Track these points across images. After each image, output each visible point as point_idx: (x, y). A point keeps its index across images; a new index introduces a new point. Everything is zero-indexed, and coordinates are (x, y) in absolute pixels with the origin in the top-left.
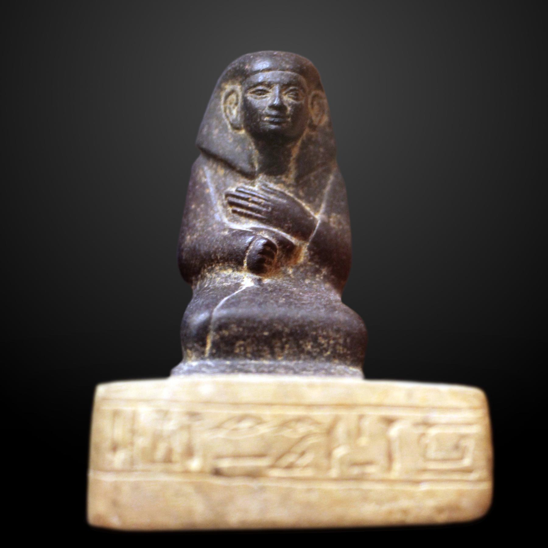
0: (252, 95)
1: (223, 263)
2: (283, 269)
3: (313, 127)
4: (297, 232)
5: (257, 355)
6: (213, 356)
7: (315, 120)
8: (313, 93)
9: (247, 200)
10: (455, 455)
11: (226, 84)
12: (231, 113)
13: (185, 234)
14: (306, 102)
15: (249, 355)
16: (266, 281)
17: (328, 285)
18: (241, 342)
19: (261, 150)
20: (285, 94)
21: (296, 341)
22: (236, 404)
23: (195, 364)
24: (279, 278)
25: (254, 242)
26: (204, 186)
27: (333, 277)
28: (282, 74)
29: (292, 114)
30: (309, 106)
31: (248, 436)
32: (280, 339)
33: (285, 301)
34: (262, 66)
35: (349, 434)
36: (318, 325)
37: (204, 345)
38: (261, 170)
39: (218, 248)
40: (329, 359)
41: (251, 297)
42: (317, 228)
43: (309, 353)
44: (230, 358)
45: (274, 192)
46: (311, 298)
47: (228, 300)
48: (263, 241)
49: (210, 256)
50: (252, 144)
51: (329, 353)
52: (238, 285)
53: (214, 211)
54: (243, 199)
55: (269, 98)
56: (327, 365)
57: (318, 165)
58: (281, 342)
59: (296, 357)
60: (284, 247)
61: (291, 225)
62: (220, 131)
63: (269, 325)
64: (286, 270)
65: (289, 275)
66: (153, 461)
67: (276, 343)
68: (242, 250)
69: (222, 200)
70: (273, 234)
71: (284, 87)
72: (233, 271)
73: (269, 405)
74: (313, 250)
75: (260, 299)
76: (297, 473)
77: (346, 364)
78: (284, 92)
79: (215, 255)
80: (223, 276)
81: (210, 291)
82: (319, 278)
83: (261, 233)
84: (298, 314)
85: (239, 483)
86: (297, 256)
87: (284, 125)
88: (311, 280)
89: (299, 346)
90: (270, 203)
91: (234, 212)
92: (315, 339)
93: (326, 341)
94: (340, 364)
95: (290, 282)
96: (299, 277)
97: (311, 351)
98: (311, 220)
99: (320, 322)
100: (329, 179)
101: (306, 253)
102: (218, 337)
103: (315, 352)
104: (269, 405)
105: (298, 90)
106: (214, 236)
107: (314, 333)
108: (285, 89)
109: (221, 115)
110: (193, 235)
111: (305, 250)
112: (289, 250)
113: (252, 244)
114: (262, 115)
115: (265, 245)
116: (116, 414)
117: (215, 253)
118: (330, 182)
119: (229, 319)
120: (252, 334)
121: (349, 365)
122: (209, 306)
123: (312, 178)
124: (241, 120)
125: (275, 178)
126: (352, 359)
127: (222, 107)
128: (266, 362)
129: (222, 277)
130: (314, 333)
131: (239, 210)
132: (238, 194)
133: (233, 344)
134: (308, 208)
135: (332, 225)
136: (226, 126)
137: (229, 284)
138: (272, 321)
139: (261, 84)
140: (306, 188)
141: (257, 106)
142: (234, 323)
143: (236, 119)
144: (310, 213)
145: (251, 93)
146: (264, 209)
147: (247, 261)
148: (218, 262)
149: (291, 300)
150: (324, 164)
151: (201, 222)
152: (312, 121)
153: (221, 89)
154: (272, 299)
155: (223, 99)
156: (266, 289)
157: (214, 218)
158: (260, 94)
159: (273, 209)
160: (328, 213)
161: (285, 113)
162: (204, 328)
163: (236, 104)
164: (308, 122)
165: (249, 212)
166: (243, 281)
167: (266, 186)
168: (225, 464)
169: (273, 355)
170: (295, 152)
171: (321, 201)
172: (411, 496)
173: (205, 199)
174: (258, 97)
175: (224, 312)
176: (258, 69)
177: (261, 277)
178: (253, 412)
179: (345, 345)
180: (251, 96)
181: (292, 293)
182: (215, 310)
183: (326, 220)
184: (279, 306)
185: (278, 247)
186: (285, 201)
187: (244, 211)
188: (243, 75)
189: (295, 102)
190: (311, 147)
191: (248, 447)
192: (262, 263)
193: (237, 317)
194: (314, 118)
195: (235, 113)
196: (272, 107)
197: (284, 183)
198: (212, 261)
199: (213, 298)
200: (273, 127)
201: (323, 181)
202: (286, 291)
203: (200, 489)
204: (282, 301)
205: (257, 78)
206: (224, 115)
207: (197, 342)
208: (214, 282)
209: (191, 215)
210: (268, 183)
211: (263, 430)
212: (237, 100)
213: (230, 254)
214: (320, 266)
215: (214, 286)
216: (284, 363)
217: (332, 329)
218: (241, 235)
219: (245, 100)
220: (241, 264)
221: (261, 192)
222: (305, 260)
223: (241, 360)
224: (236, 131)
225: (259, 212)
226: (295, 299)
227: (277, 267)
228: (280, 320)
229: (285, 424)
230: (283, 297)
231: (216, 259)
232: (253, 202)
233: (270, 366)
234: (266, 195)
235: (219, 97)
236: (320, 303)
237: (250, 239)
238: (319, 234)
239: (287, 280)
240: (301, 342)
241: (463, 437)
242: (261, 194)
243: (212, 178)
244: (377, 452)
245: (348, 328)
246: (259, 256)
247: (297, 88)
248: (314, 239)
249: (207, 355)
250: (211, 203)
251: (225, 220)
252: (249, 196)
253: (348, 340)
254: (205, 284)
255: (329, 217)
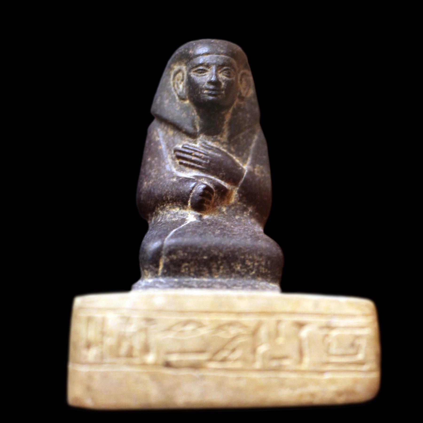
0: (195, 73)
1: (172, 203)
2: (218, 207)
3: (242, 98)
4: (229, 179)
5: (198, 274)
6: (164, 275)
7: (244, 93)
8: (242, 72)
9: (190, 154)
10: (351, 351)
11: (175, 65)
12: (178, 87)
13: (143, 181)
14: (236, 79)
15: (192, 274)
16: (206, 217)
17: (253, 220)
18: (186, 264)
19: (202, 116)
20: (220, 73)
21: (229, 263)
22: (182, 312)
23: (150, 281)
24: (215, 215)
25: (196, 187)
26: (158, 143)
27: (257, 214)
28: (218, 57)
29: (225, 88)
30: (239, 82)
31: (192, 337)
32: (216, 262)
33: (220, 232)
34: (203, 50)
35: (269, 335)
36: (245, 251)
37: (158, 266)
38: (202, 131)
39: (168, 192)
40: (254, 277)
41: (194, 229)
42: (244, 176)
43: (238, 272)
44: (178, 276)
45: (211, 148)
46: (240, 230)
47: (176, 232)
48: (203, 186)
49: (162, 197)
50: (195, 111)
51: (254, 272)
52: (183, 220)
53: (165, 163)
54: (187, 153)
55: (207, 76)
56: (253, 282)
57: (245, 128)
58: (217, 264)
59: (228, 276)
60: (220, 191)
61: (224, 174)
62: (170, 102)
63: (208, 251)
64: (221, 208)
65: (223, 213)
66: (118, 356)
67: (213, 265)
68: (186, 193)
69: (172, 155)
70: (211, 181)
71: (220, 67)
72: (180, 209)
73: (208, 312)
74: (242, 193)
75: (200, 231)
76: (229, 365)
77: (267, 281)
78: (219, 71)
79: (166, 197)
80: (172, 213)
81: (162, 225)
82: (246, 214)
83: (201, 180)
84: (230, 242)
85: (184, 372)
86: (229, 198)
87: (219, 96)
88: (240, 216)
89: (231, 267)
90: (208, 157)
91: (181, 163)
92: (243, 262)
93: (252, 263)
94: (262, 281)
95: (224, 217)
96: (231, 214)
97: (240, 271)
98: (240, 170)
99: (247, 249)
100: (254, 138)
101: (236, 195)
102: (168, 260)
103: (243, 271)
104: (208, 312)
105: (230, 70)
106: (165, 182)
107: (243, 257)
108: (220, 69)
109: (171, 89)
110: (149, 181)
111: (235, 193)
112: (223, 193)
113: (195, 189)
114: (202, 89)
115: (204, 189)
116: (89, 319)
117: (166, 195)
118: (254, 140)
119: (177, 246)
120: (195, 258)
121: (270, 282)
122: (162, 237)
123: (241, 138)
124: (186, 92)
125: (212, 138)
126: (271, 277)
127: (172, 83)
128: (205, 280)
129: (172, 214)
130: (243, 257)
131: (184, 162)
132: (184, 150)
133: (180, 266)
134: (237, 161)
135: (256, 173)
136: (175, 98)
137: (177, 219)
138: (210, 248)
139: (202, 65)
140: (236, 145)
141: (198, 82)
142: (181, 249)
143: (182, 92)
144: (239, 165)
145: (194, 72)
146: (204, 162)
147: (191, 201)
148: (169, 203)
149: (225, 232)
150: (250, 127)
151: (155, 171)
152: (241, 94)
153: (171, 69)
154: (210, 231)
155: (172, 76)
156: (206, 223)
157: (165, 168)
158: (201, 73)
159: (211, 161)
160: (253, 164)
161: (220, 87)
162: (158, 253)
163: (182, 80)
164: (238, 94)
165: (192, 164)
166: (187, 217)
167: (205, 143)
168: (174, 358)
169: (211, 274)
170: (228, 117)
171: (248, 155)
172: (317, 383)
173: (158, 154)
174: (199, 75)
175: (173, 241)
176: (199, 53)
177: (201, 214)
178: (195, 318)
179: (266, 267)
180: (194, 74)
181: (225, 226)
182: (166, 239)
183: (252, 170)
184: (215, 237)
185: (214, 191)
186: (220, 155)
187: (188, 163)
188: (188, 58)
189: (228, 79)
190: (240, 114)
191: (191, 345)
192: (202, 203)
193: (183, 245)
194: (242, 91)
195: (181, 87)
196: (210, 82)
197: (219, 141)
198: (164, 201)
199: (164, 230)
200: (211, 98)
201: (249, 140)
202: (221, 225)
203: (154, 377)
204: (218, 232)
205: (199, 60)
206: (173, 89)
207: (152, 264)
208: (165, 218)
209: (148, 166)
210: (207, 141)
211: (203, 332)
212: (183, 77)
213: (178, 196)
214: (247, 205)
215: (166, 221)
216: (219, 280)
217: (256, 254)
218: (186, 181)
219: (189, 77)
220: (186, 204)
221: (202, 148)
222: (235, 201)
223: (186, 278)
224: (182, 101)
225: (200, 163)
226: (228, 231)
227: (214, 206)
228: (216, 247)
229: (220, 327)
230: (219, 229)
231: (167, 200)
232: (195, 156)
233: (208, 282)
234: (206, 150)
235: (169, 75)
236: (247, 234)
237: (193, 184)
238: (246, 180)
239: (222, 216)
240: (232, 264)
241: (358, 337)
242: (202, 150)
243: (164, 137)
244: (291, 349)
245: (269, 253)
246: (200, 198)
247: (229, 68)
248: (242, 184)
249: (160, 274)
250: (163, 157)
251: (174, 170)
252: (193, 152)
253: (269, 263)
254: (158, 219)
255: (254, 168)
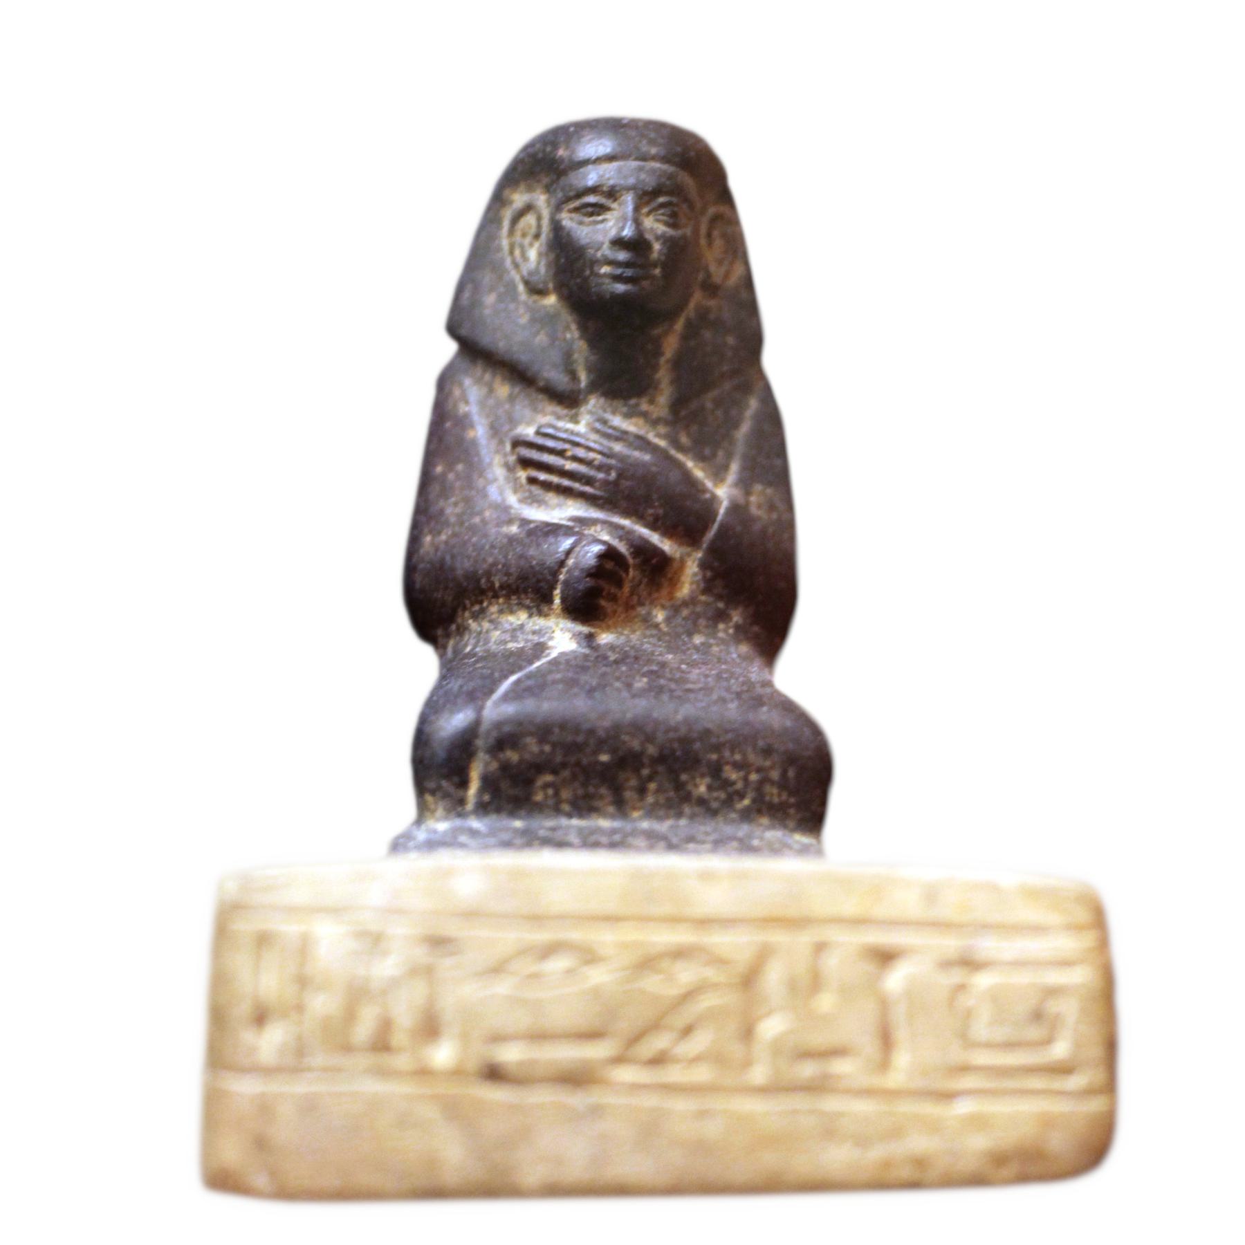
0: (573, 215)
1: (508, 597)
2: (642, 611)
4: (675, 527)
5: (584, 806)
6: (483, 808)
8: (712, 211)
9: (561, 453)
10: (1034, 1033)
11: (515, 191)
12: (525, 257)
14: (696, 231)
15: (566, 807)
16: (605, 638)
17: (744, 648)
18: (549, 778)
19: (594, 341)
20: (648, 214)
21: (674, 774)
22: (537, 919)
24: (634, 632)
25: (577, 549)
27: (756, 629)
28: (640, 169)
29: (663, 258)
30: (703, 242)
31: (564, 991)
32: (637, 770)
33: (648, 683)
35: (792, 986)
36: (722, 739)
37: (464, 784)
38: (594, 387)
39: (495, 564)
40: (747, 816)
41: (570, 675)
42: (719, 518)
43: (702, 802)
44: (523, 813)
45: (622, 436)
46: (707, 676)
47: (518, 682)
48: (597, 549)
49: (478, 581)
50: (574, 327)
51: (746, 802)
52: (540, 649)
53: (485, 478)
54: (551, 451)
55: (611, 224)
56: (744, 830)
57: (722, 376)
58: (639, 777)
59: (672, 812)
60: (646, 561)
61: (661, 512)
62: (500, 299)
63: (611, 739)
64: (649, 613)
65: (657, 626)
66: (348, 1048)
67: (627, 780)
68: (549, 568)
69: (505, 455)
70: (621, 533)
71: (646, 198)
72: (530, 616)
73: (612, 919)
74: (711, 568)
75: (590, 679)
76: (674, 1074)
77: (785, 827)
78: (645, 210)
79: (489, 580)
80: (507, 626)
81: (477, 662)
82: (725, 631)
83: (593, 528)
84: (676, 713)
85: (542, 1096)
86: (674, 583)
87: (645, 283)
88: (706, 635)
89: (679, 786)
90: (613, 462)
91: (532, 481)
92: (715, 771)
93: (742, 774)
94: (772, 827)
95: (659, 640)
96: (680, 630)
97: (706, 796)
98: (706, 500)
99: (727, 732)
100: (747, 406)
101: (695, 574)
102: (494, 766)
103: (716, 799)
104: (612, 919)
105: (676, 205)
106: (486, 535)
107: (714, 757)
108: (648, 203)
109: (502, 261)
110: (439, 533)
111: (692, 568)
112: (657, 569)
113: (573, 555)
114: (594, 262)
115: (602, 557)
117: (488, 574)
118: (749, 413)
119: (520, 724)
120: (573, 759)
121: (794, 830)
123: (709, 405)
124: (547, 272)
125: (625, 405)
126: (799, 816)
127: (505, 243)
128: (605, 823)
130: (714, 757)
131: (543, 476)
132: (540, 441)
133: (529, 782)
134: (699, 474)
135: (754, 511)
136: (514, 287)
137: (521, 645)
138: (617, 729)
139: (593, 190)
140: (694, 428)
141: (584, 241)
142: (531, 734)
143: (537, 271)
144: (704, 485)
145: (570, 211)
146: (601, 476)
147: (562, 592)
148: (496, 596)
149: (662, 682)
150: (735, 373)
151: (456, 504)
152: (709, 275)
154: (618, 679)
155: (506, 224)
156: (605, 658)
157: (485, 496)
158: (591, 214)
159: (620, 475)
160: (745, 483)
161: (647, 257)
163: (537, 236)
164: (701, 276)
165: (566, 482)
166: (551, 638)
167: (605, 422)
168: (511, 1054)
169: (621, 807)
170: (671, 345)
171: (729, 456)
172: (934, 1127)
174: (587, 220)
175: (510, 709)
176: (587, 157)
177: (593, 630)
178: (575, 935)
179: (783, 785)
180: (571, 219)
181: (663, 665)
182: (489, 703)
183: (741, 501)
184: (634, 696)
185: (631, 561)
186: (647, 457)
187: (555, 479)
189: (670, 232)
190: (707, 334)
191: (562, 1015)
192: (595, 596)
193: (538, 720)
194: (713, 268)
195: (534, 256)
196: (619, 243)
197: (645, 415)
198: (483, 592)
199: (483, 677)
200: (620, 288)
201: (734, 412)
202: (649, 662)
203: (453, 1110)
204: (641, 683)
205: (585, 176)
206: (508, 261)
207: (447, 777)
208: (487, 641)
210: (608, 416)
211: (598, 976)
212: (539, 226)
213: (523, 577)
214: (727, 604)
215: (487, 651)
216: (645, 825)
217: (754, 747)
218: (547, 534)
219: (557, 227)
220: (548, 599)
221: (594, 436)
222: (692, 592)
223: (548, 817)
224: (535, 297)
225: (589, 481)
226: (671, 680)
227: (629, 607)
228: (636, 727)
229: (647, 963)
230: (644, 675)
231: (492, 587)
232: (575, 459)
233: (614, 831)
234: (605, 442)
236: (728, 689)
237: (567, 543)
238: (724, 531)
239: (652, 636)
240: (684, 777)
241: (1053, 992)
242: (594, 440)
243: (482, 404)
244: (856, 1027)
245: (791, 746)
246: (589, 582)
247: (674, 200)
248: (713, 542)
249: (470, 806)
250: (480, 461)
251: (512, 499)
252: (567, 446)
253: (791, 773)
254: (466, 645)
255: (748, 493)
